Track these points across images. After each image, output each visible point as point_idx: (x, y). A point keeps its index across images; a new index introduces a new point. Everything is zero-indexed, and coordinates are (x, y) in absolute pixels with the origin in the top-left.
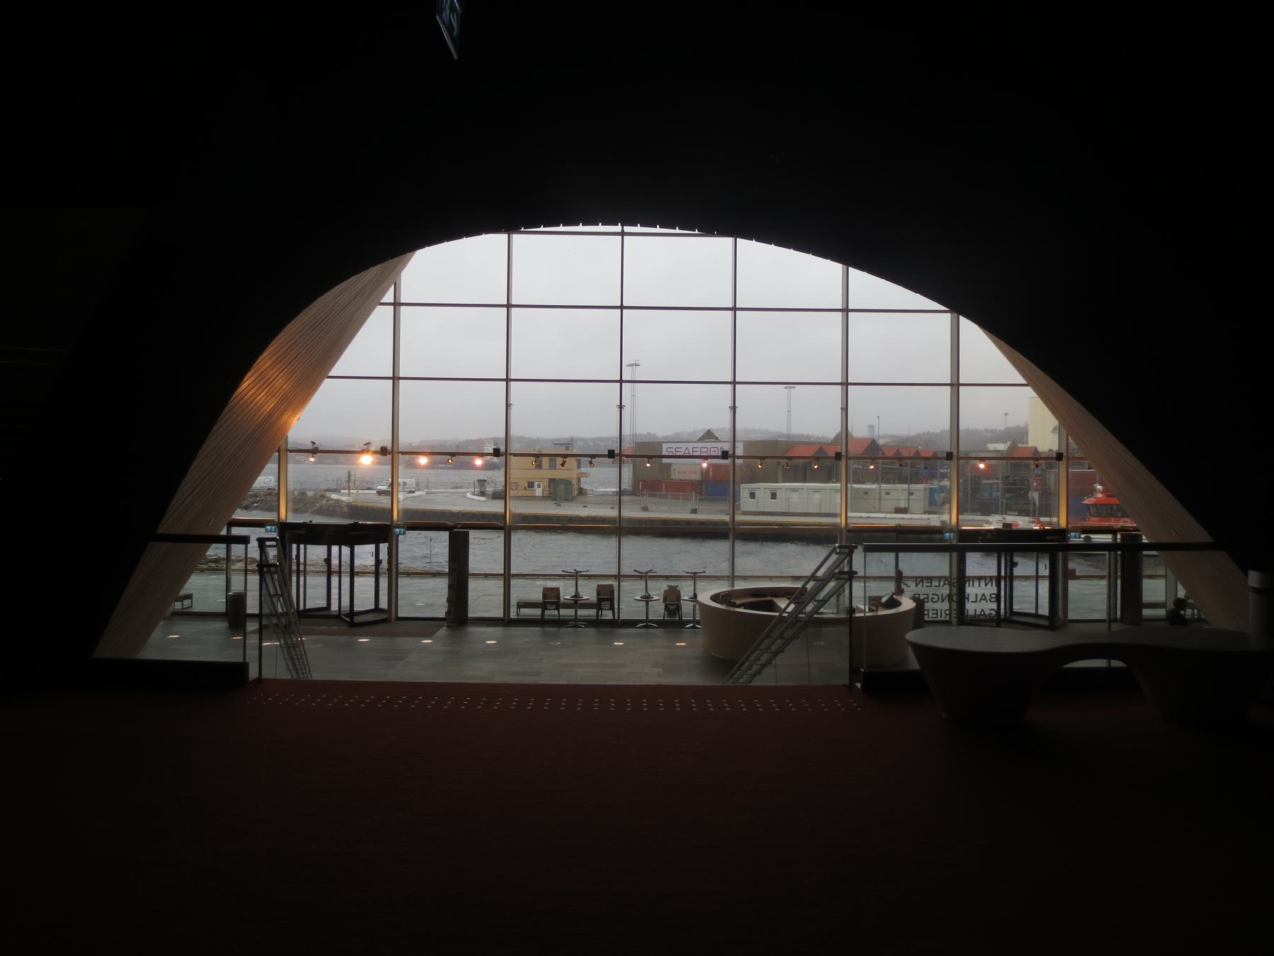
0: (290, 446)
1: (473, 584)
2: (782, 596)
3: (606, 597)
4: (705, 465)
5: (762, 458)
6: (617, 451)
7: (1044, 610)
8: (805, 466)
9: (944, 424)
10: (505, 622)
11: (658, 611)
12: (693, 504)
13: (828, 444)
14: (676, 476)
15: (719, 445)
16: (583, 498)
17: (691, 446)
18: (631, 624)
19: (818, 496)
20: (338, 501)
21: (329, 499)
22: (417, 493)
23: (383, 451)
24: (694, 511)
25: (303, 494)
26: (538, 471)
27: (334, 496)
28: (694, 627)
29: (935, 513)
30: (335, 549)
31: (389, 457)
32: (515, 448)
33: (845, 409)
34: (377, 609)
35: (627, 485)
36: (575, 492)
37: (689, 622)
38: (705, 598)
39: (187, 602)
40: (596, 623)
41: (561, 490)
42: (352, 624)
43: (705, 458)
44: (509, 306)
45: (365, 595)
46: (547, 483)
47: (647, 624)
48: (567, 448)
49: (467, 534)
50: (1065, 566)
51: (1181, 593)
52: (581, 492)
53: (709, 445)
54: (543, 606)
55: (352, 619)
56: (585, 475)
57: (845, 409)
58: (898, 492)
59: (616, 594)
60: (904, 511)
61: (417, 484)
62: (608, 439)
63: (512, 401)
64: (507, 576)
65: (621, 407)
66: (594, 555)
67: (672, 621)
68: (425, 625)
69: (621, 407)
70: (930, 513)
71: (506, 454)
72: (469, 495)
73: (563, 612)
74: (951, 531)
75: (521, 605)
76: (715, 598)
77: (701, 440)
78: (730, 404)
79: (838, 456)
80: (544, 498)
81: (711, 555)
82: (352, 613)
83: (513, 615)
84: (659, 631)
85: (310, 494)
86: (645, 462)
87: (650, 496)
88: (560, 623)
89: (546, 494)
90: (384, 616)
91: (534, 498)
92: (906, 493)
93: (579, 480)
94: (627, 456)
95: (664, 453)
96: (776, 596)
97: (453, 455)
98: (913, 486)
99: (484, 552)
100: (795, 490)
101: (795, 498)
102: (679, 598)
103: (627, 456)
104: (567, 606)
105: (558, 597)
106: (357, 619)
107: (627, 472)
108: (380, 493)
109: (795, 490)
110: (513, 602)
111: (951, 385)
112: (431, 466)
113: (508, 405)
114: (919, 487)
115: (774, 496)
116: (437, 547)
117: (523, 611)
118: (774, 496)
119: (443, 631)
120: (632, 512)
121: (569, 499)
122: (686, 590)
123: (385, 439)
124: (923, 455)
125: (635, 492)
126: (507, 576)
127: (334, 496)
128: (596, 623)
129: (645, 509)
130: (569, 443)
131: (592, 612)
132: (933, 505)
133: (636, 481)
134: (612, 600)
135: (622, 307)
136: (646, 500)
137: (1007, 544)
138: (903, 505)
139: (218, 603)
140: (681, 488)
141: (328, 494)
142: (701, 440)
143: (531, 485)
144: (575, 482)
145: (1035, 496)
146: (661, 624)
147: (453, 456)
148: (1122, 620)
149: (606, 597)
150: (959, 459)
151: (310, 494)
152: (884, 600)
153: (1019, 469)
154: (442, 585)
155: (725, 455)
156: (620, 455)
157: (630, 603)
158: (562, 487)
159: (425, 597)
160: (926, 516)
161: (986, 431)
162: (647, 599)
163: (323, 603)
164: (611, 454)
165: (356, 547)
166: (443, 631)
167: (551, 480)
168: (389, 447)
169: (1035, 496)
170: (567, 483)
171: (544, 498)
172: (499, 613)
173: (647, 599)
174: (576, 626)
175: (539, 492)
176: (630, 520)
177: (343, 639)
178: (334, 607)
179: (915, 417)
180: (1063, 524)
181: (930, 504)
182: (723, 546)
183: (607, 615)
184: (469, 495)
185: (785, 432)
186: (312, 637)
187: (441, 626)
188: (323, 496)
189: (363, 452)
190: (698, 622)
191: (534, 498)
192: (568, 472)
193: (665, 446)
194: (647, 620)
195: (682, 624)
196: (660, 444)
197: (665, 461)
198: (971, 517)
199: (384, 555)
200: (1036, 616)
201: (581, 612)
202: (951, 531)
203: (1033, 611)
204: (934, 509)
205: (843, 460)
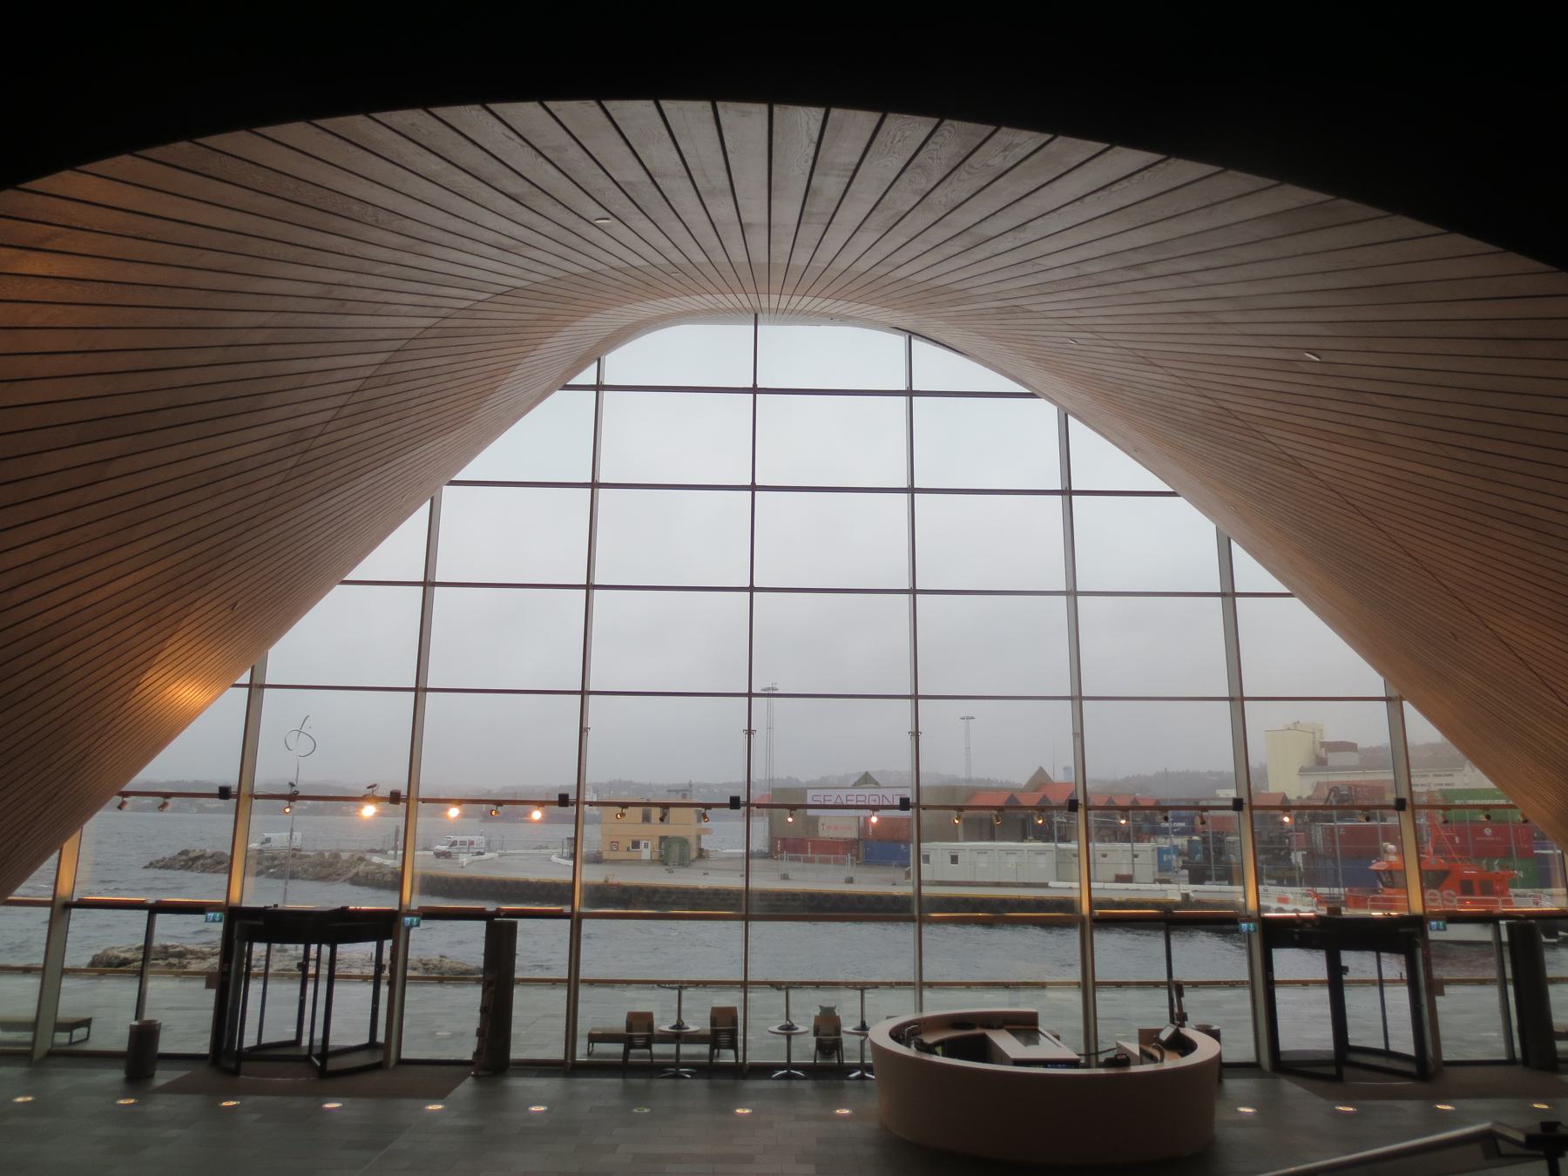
0: (257, 791)
1: (520, 996)
2: (999, 1027)
3: (725, 1028)
4: (874, 820)
5: (960, 809)
6: (743, 799)
7: (1403, 1042)
8: (1024, 821)
9: (1223, 760)
10: (567, 1068)
11: (805, 1050)
12: (849, 870)
13: (1021, 791)
14: (825, 833)
15: (880, 792)
16: (702, 863)
17: (843, 793)
18: (764, 1071)
19: (1012, 859)
20: (380, 866)
21: (369, 863)
22: (487, 855)
23: (395, 798)
24: (850, 881)
25: (336, 856)
26: (647, 826)
27: (376, 859)
28: (862, 1077)
29: (1168, 882)
30: (314, 947)
31: (402, 805)
32: (590, 796)
33: (1079, 736)
34: (372, 1045)
35: (760, 842)
36: (694, 854)
37: (854, 1068)
38: (880, 1035)
39: (80, 1033)
40: (707, 1070)
41: (673, 852)
42: (323, 1074)
43: (875, 808)
44: (589, 587)
45: (351, 1018)
46: (656, 842)
47: (789, 1071)
48: (684, 796)
49: (514, 925)
50: (1429, 975)
51: (245, 678)
52: (701, 854)
53: (867, 792)
54: (628, 1040)
55: (324, 1063)
56: (707, 831)
57: (1079, 736)
58: (1115, 855)
59: (740, 1038)
60: (1127, 879)
61: (488, 843)
62: (730, 785)
63: (591, 722)
64: (573, 983)
65: (749, 732)
66: (709, 948)
67: (828, 1067)
68: (437, 1075)
69: (749, 732)
70: (1161, 881)
71: (577, 802)
72: (554, 858)
73: (657, 1049)
74: (1248, 919)
75: (593, 1038)
76: (897, 1034)
77: (855, 786)
78: (909, 727)
79: (1073, 806)
80: (651, 862)
81: (877, 949)
82: (326, 1053)
83: (581, 1055)
84: (807, 1086)
85: (345, 856)
86: (788, 816)
87: (792, 859)
88: (653, 1070)
89: (656, 856)
90: (378, 1057)
91: (639, 862)
92: (1129, 855)
93: (699, 838)
94: (759, 806)
95: (810, 802)
96: (991, 1027)
97: (499, 803)
98: (1138, 846)
99: (540, 945)
100: (1010, 852)
101: (982, 862)
102: (837, 1030)
103: (759, 806)
104: (665, 1038)
105: (650, 1026)
106: (333, 1064)
107: (760, 826)
108: (439, 855)
109: (1010, 852)
110: (584, 1026)
111: (1231, 699)
112: (546, 820)
113: (583, 730)
114: (1146, 848)
115: (954, 859)
116: (465, 943)
117: (601, 1048)
118: (954, 859)
119: (466, 1087)
120: (765, 880)
121: (684, 862)
122: (847, 1008)
123: (397, 780)
124: (1142, 804)
125: (770, 855)
126: (573, 983)
127: (376, 859)
128: (707, 1070)
129: (785, 877)
130: (687, 789)
131: (704, 1049)
132: (1164, 873)
133: (773, 840)
134: (734, 1033)
135: (752, 589)
136: (786, 865)
137: (1330, 936)
138: (1125, 871)
139: (113, 1034)
140: (833, 849)
141: (368, 857)
142: (855, 786)
143: (636, 845)
144: (693, 841)
145: (1297, 858)
146: (811, 1071)
147: (497, 805)
148: (1526, 1061)
149: (725, 1028)
150: (1252, 808)
151: (345, 856)
152: (1164, 1036)
153: (1346, 824)
154: (471, 997)
155: (905, 804)
156: (748, 804)
157: (761, 1044)
158: (676, 848)
159: (443, 1022)
160: (1157, 886)
161: (1210, 773)
162: (788, 1030)
163: (289, 1034)
164: (735, 803)
165: (341, 948)
166: (466, 1087)
167: (663, 839)
168: (404, 793)
169: (1297, 858)
170: (683, 842)
171: (651, 862)
172: (556, 1052)
173: (788, 1030)
174: (678, 1076)
175: (645, 854)
176: (764, 895)
177: (298, 1103)
178: (305, 1041)
179: (1180, 749)
180: (1417, 908)
181: (1161, 870)
182: (902, 934)
183: (727, 1057)
184: (554, 858)
185: (962, 775)
186: (250, 1100)
187: (463, 1077)
188: (361, 859)
189: (365, 799)
190: (869, 1069)
191: (639, 862)
192: (682, 824)
193: (810, 793)
194: (789, 1066)
195: (842, 1071)
196: (804, 791)
197: (810, 812)
198: (1217, 888)
199: (386, 955)
200: (1387, 1053)
201: (686, 1049)
202: (1248, 919)
203: (1382, 1046)
204: (1165, 876)
205: (1081, 811)
